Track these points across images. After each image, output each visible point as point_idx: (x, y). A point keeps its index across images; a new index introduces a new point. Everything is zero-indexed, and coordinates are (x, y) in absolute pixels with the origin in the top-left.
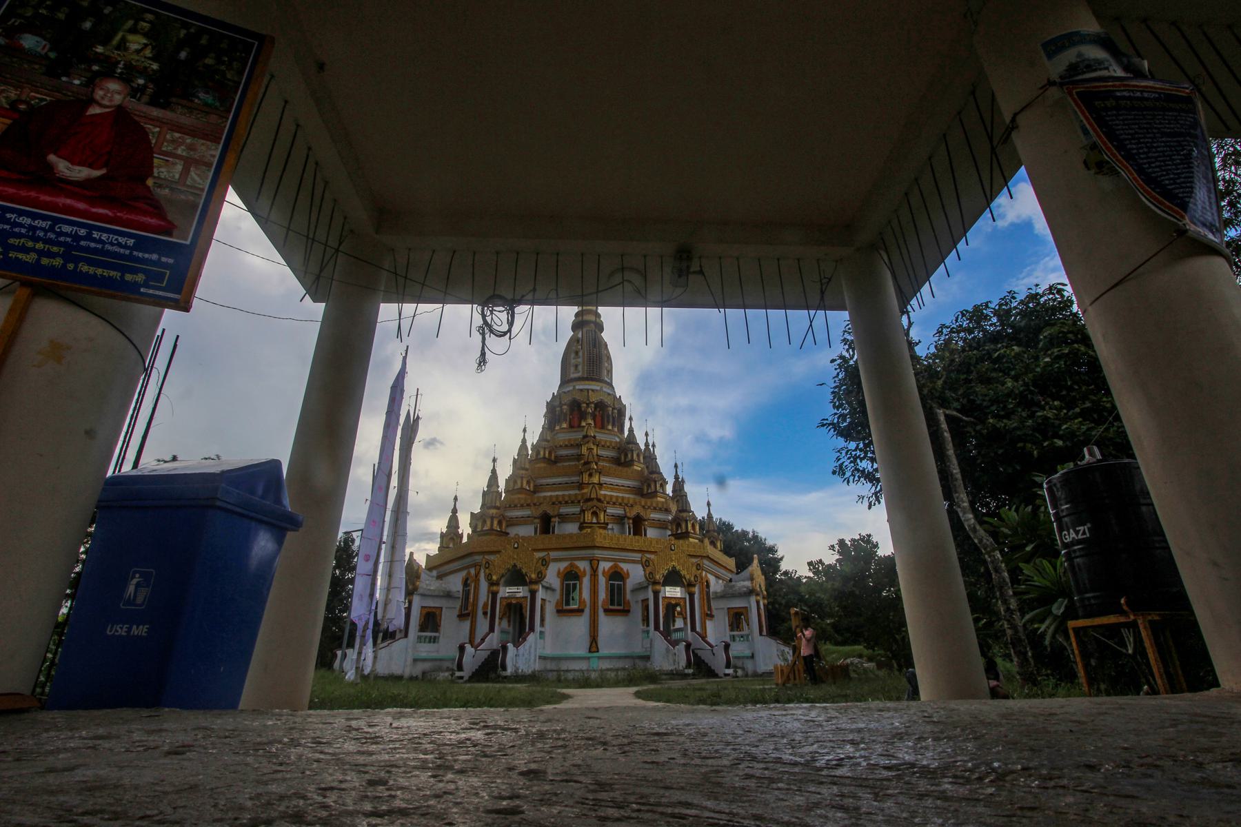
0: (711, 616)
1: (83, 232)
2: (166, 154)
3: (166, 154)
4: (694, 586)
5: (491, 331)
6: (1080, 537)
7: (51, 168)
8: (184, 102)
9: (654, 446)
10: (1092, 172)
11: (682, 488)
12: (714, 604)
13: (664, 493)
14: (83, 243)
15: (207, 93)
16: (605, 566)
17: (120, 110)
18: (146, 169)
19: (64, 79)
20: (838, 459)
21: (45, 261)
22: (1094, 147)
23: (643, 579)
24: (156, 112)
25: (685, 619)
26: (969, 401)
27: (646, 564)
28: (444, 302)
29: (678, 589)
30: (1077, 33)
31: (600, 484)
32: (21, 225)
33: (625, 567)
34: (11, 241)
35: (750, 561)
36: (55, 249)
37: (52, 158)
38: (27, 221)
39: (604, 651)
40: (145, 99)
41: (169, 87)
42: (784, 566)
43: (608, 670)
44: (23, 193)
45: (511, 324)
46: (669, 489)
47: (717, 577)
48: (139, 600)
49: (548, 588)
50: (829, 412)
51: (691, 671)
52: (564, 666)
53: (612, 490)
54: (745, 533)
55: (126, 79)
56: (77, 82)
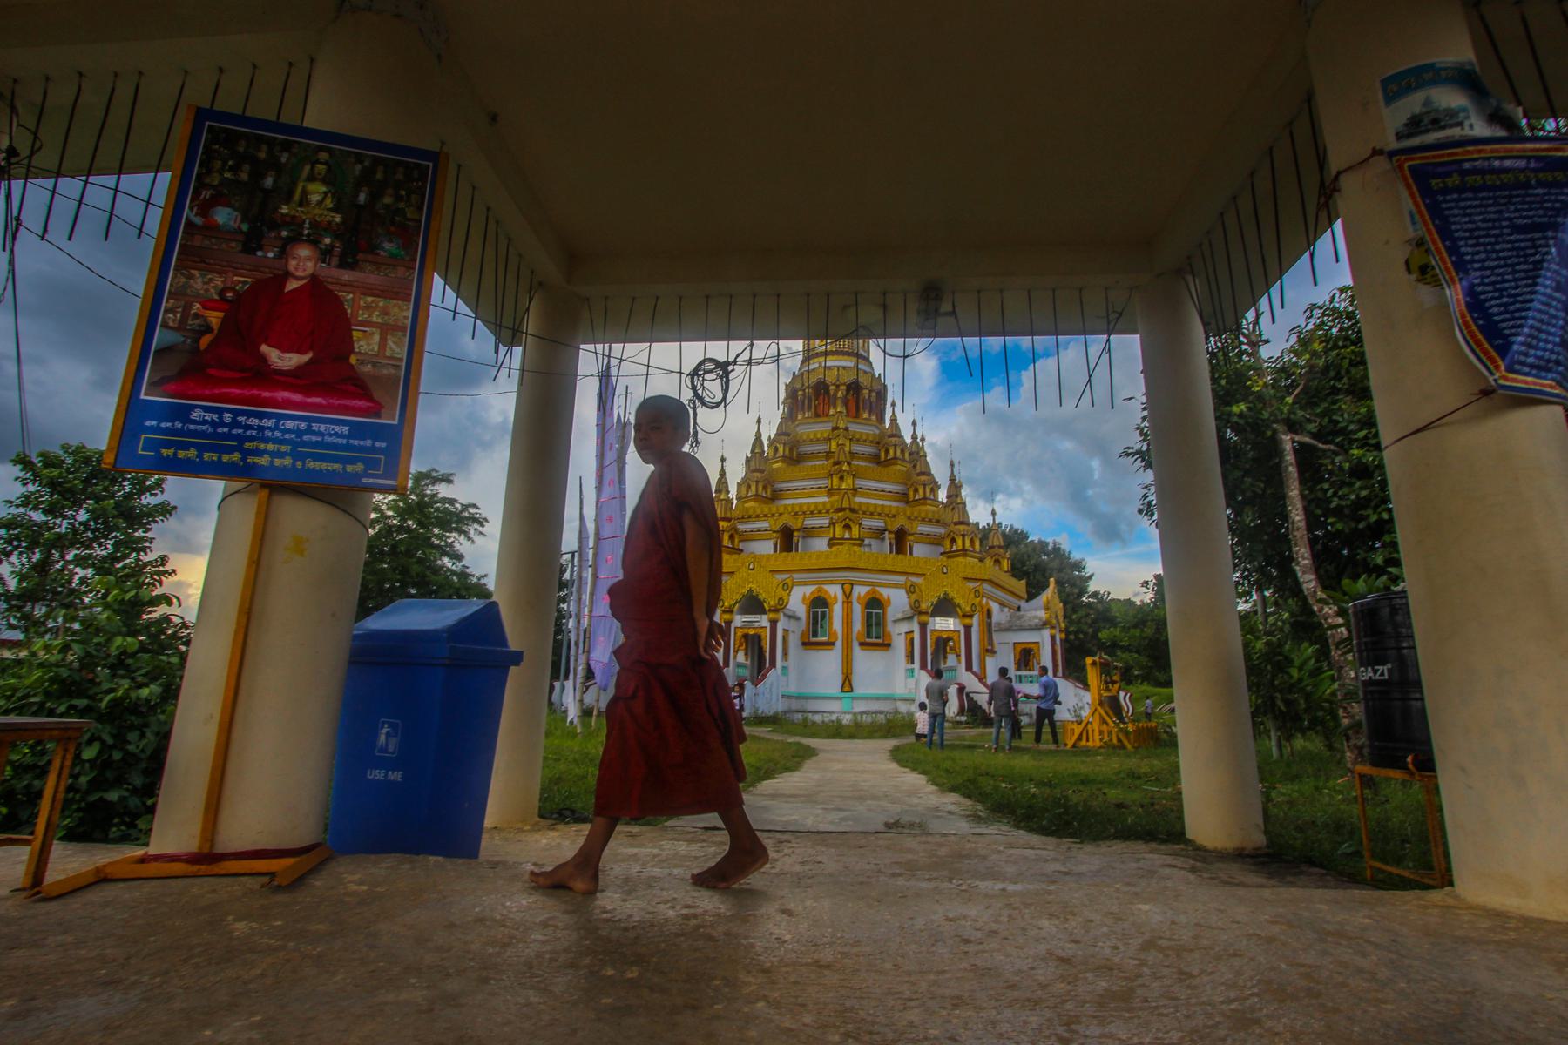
0: (992, 652)
1: (303, 426)
2: (362, 323)
3: (362, 323)
4: (971, 616)
5: (704, 404)
6: (1378, 677)
7: (264, 359)
8: (370, 257)
9: (923, 439)
10: (1414, 277)
11: (958, 495)
12: (996, 637)
13: (936, 500)
14: (305, 438)
15: (390, 241)
16: (861, 591)
17: (314, 279)
18: (346, 345)
19: (259, 253)
20: (1145, 496)
21: (277, 462)
22: (1420, 243)
23: (907, 608)
24: (346, 275)
25: (958, 656)
26: (1331, 421)
27: (911, 590)
28: (651, 342)
29: (951, 621)
30: (1430, 67)
31: (855, 490)
32: (250, 427)
33: (884, 592)
34: (247, 445)
35: (1044, 587)
36: (283, 448)
37: (264, 348)
38: (254, 421)
39: (859, 690)
40: (335, 261)
41: (352, 244)
42: (1092, 587)
43: (862, 713)
44: (247, 393)
45: (725, 391)
46: (942, 496)
47: (1002, 605)
48: (391, 749)
49: (792, 617)
50: (1135, 441)
51: (964, 718)
52: (811, 706)
53: (869, 497)
54: (1043, 544)
55: (314, 242)
56: (271, 255)
